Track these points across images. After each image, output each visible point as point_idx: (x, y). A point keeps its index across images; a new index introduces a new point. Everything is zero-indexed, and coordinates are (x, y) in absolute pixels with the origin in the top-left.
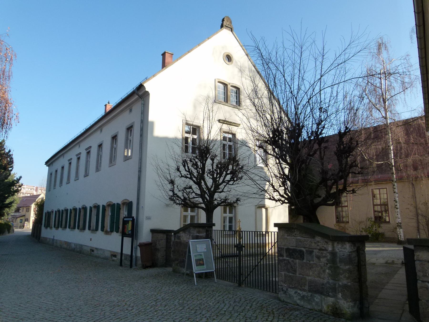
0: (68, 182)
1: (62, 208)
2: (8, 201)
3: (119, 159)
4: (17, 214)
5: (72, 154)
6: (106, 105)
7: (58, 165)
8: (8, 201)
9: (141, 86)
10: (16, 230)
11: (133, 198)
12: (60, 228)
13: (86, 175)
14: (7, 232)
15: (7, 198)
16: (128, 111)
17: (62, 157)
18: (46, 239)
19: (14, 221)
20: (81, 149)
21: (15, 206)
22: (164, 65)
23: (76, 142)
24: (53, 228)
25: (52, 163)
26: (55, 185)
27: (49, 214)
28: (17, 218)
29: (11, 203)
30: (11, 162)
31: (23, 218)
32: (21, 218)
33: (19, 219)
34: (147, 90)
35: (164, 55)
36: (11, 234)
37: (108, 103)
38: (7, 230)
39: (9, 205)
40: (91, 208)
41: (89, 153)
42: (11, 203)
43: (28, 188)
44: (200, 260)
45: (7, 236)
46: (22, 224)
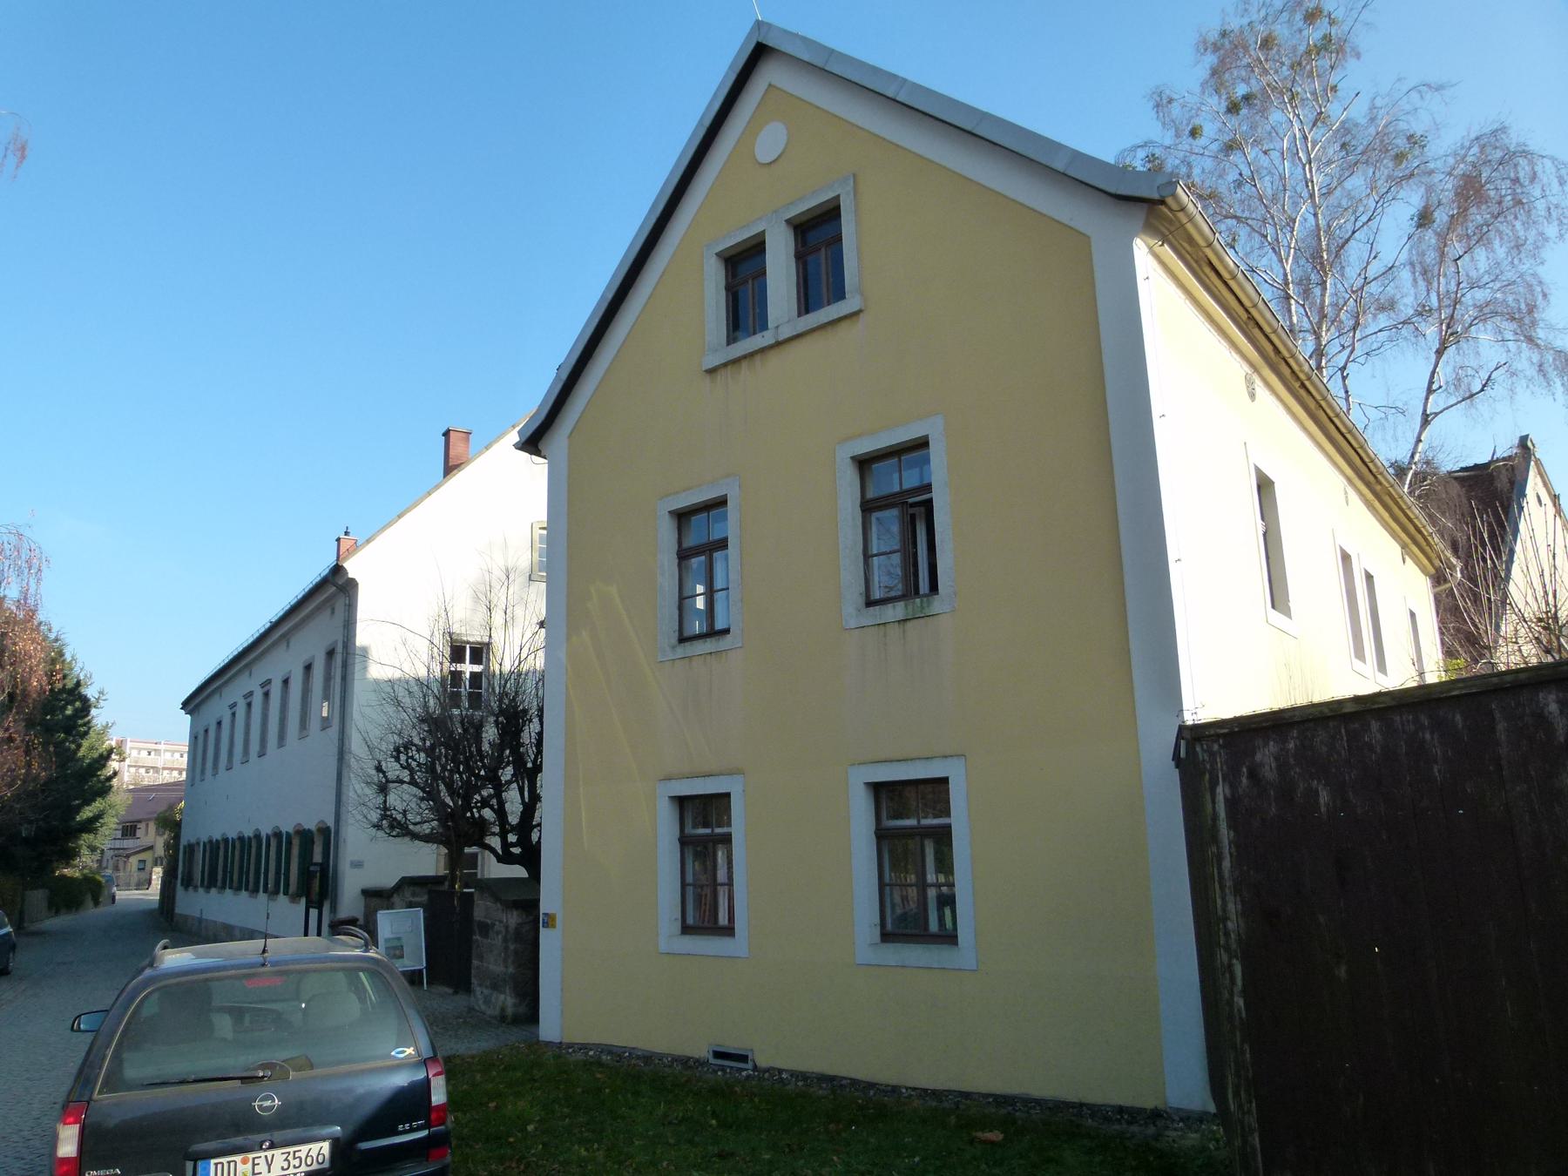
0: (215, 774)
1: (217, 836)
2: (87, 813)
3: (314, 725)
4: (129, 843)
5: (235, 692)
6: (338, 540)
7: (217, 708)
8: (87, 813)
9: (338, 570)
10: (121, 895)
11: (331, 823)
12: (228, 891)
13: (262, 754)
14: (90, 903)
15: (78, 809)
16: (329, 611)
17: (217, 696)
18: (186, 917)
19: (121, 865)
20: (250, 683)
21: (110, 824)
22: (450, 469)
23: (243, 663)
24: (201, 890)
25: (197, 706)
26: (203, 772)
27: (191, 849)
28: (128, 856)
29: (98, 817)
30: (85, 706)
31: (146, 856)
32: (142, 856)
33: (134, 860)
34: (351, 575)
35: (447, 434)
36: (101, 909)
37: (346, 533)
38: (89, 897)
39: (90, 826)
40: (268, 837)
41: (267, 695)
42: (98, 817)
43: (173, 752)
44: (395, 948)
45: (91, 913)
46: (143, 875)
